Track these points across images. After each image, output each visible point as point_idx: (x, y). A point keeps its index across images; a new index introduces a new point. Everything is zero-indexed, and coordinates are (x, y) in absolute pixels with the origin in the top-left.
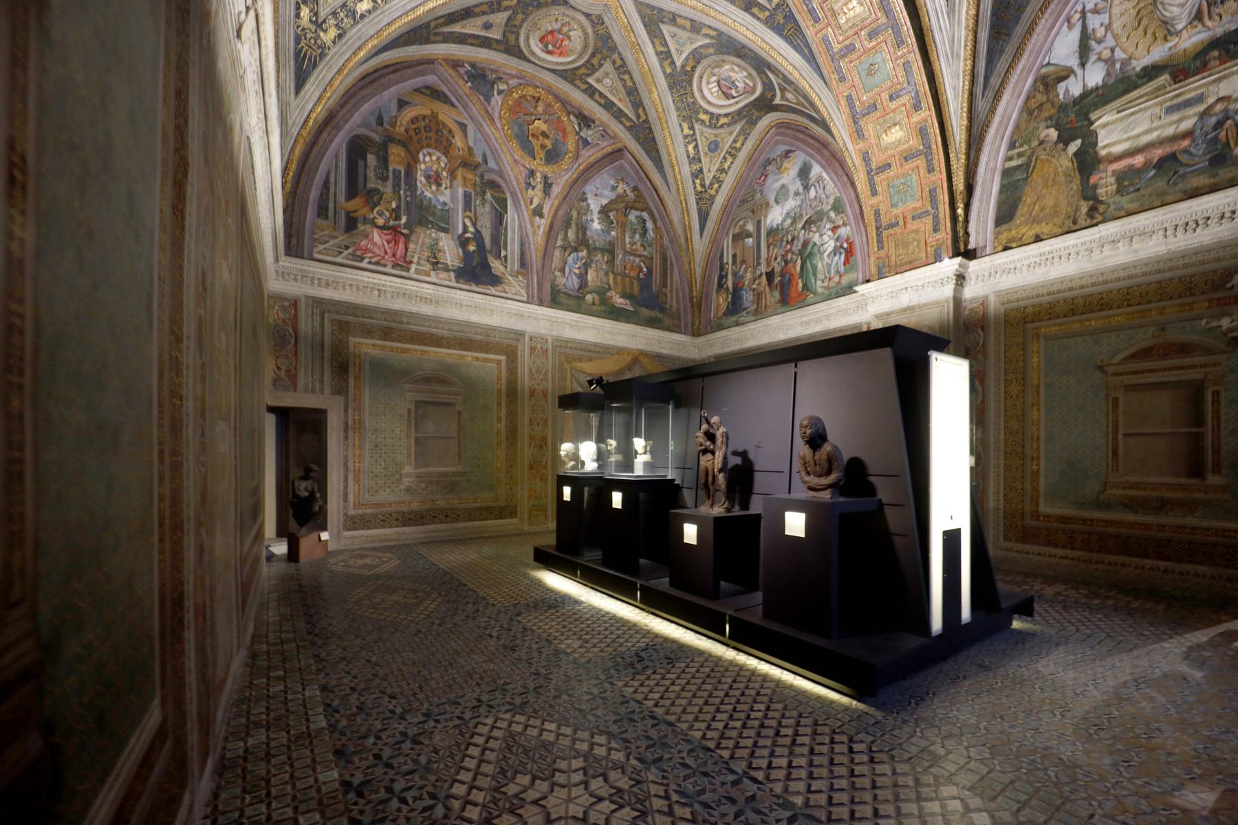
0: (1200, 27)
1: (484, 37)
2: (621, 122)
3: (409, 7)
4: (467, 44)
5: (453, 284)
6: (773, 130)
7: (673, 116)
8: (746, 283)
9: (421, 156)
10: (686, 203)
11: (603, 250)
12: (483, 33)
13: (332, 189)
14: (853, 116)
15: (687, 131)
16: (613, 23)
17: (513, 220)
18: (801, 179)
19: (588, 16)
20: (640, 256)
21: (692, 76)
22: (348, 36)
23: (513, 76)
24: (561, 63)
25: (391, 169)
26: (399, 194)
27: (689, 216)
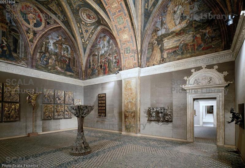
0: (180, 25)
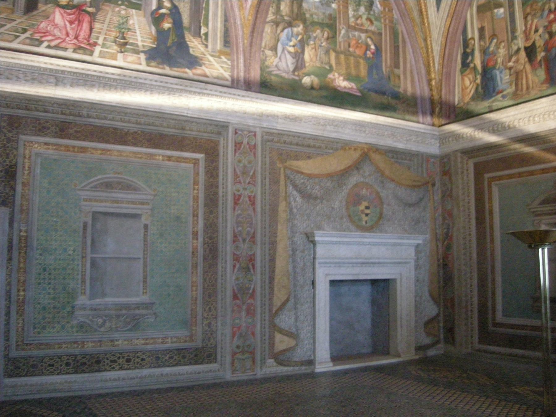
5: (144, 67)
11: (322, 25)
20: (366, 31)
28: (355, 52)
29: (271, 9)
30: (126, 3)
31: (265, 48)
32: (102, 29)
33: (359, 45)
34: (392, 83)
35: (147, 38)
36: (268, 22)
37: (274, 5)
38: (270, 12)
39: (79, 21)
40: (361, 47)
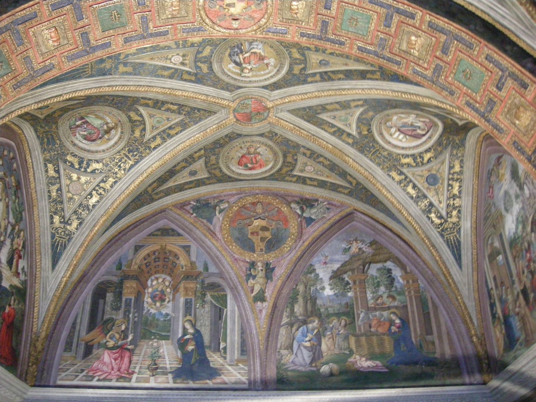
1: (195, 180)
2: (340, 192)
3: (124, 188)
4: (186, 189)
5: (171, 385)
6: (483, 143)
7: (379, 172)
8: (511, 307)
9: (149, 283)
10: (428, 239)
11: (338, 315)
12: (193, 178)
13: (78, 328)
14: (483, 116)
15: (398, 178)
16: (284, 131)
17: (233, 311)
18: (515, 181)
19: (262, 135)
20: (389, 308)
21: (373, 136)
22: (86, 222)
23: (232, 195)
24: (266, 172)
25: (124, 299)
26: (128, 317)
27: (437, 250)
28: (377, 331)
29: (285, 313)
30: (158, 337)
31: (280, 349)
32: (138, 360)
33: (382, 323)
34: (425, 350)
35: (175, 361)
36: (283, 325)
37: (288, 310)
38: (284, 316)
39: (122, 357)
40: (384, 324)
